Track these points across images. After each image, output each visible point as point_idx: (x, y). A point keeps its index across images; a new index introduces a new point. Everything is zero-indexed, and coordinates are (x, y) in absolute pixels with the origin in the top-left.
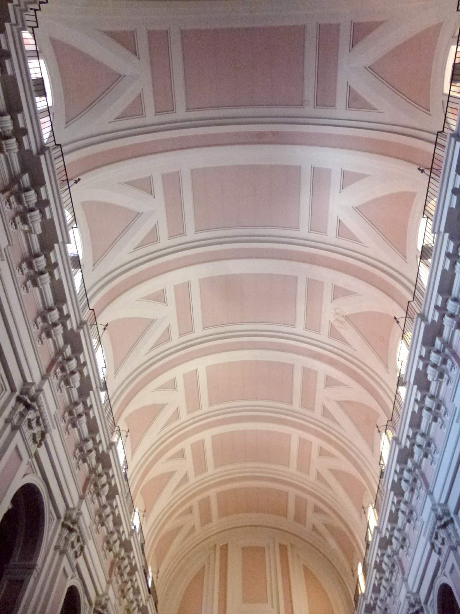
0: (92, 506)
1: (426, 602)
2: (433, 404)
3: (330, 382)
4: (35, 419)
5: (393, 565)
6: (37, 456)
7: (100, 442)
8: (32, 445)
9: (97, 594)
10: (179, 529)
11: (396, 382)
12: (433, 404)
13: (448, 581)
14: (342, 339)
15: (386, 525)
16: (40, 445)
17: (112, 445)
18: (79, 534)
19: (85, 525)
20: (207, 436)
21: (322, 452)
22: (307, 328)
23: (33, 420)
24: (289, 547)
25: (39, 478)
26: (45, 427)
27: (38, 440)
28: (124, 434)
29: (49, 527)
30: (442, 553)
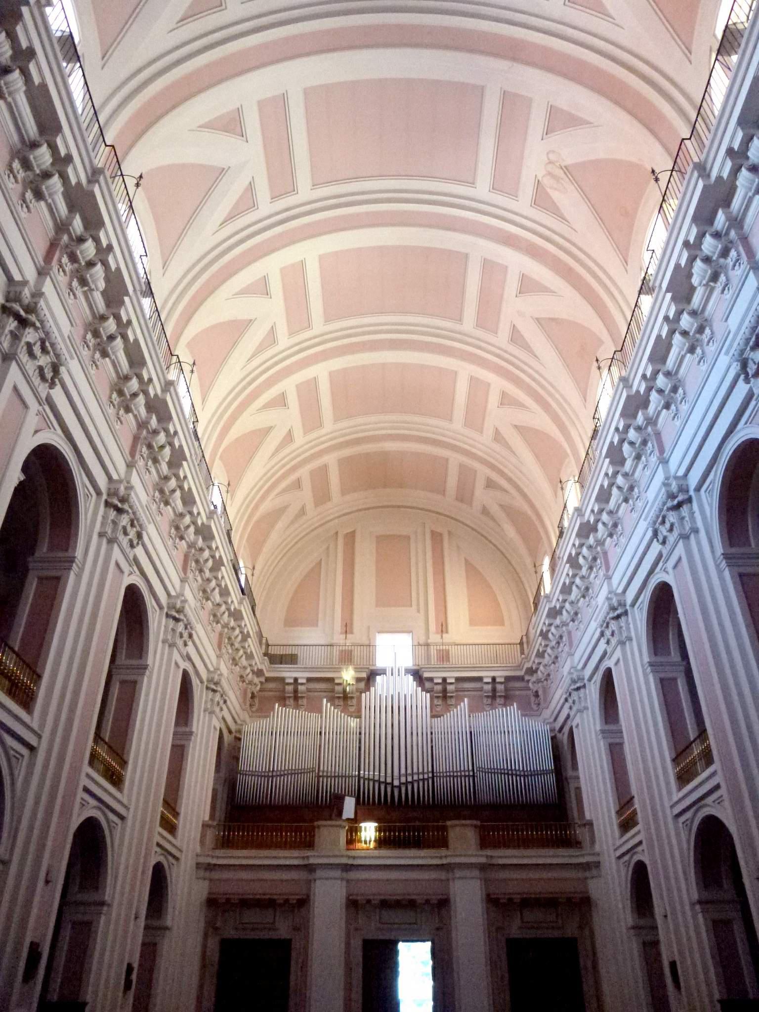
0: (147, 477)
3: (527, 286)
4: (39, 343)
6: (50, 402)
7: (150, 380)
8: (39, 384)
11: (638, 288)
13: (670, 579)
14: (527, 347)
15: (592, 504)
16: (52, 385)
18: (132, 516)
19: (62, 335)
20: (321, 371)
22: (494, 188)
23: (35, 344)
25: (137, 576)
26: (57, 356)
27: (49, 375)
28: (187, 368)
29: (85, 506)
30: (667, 542)
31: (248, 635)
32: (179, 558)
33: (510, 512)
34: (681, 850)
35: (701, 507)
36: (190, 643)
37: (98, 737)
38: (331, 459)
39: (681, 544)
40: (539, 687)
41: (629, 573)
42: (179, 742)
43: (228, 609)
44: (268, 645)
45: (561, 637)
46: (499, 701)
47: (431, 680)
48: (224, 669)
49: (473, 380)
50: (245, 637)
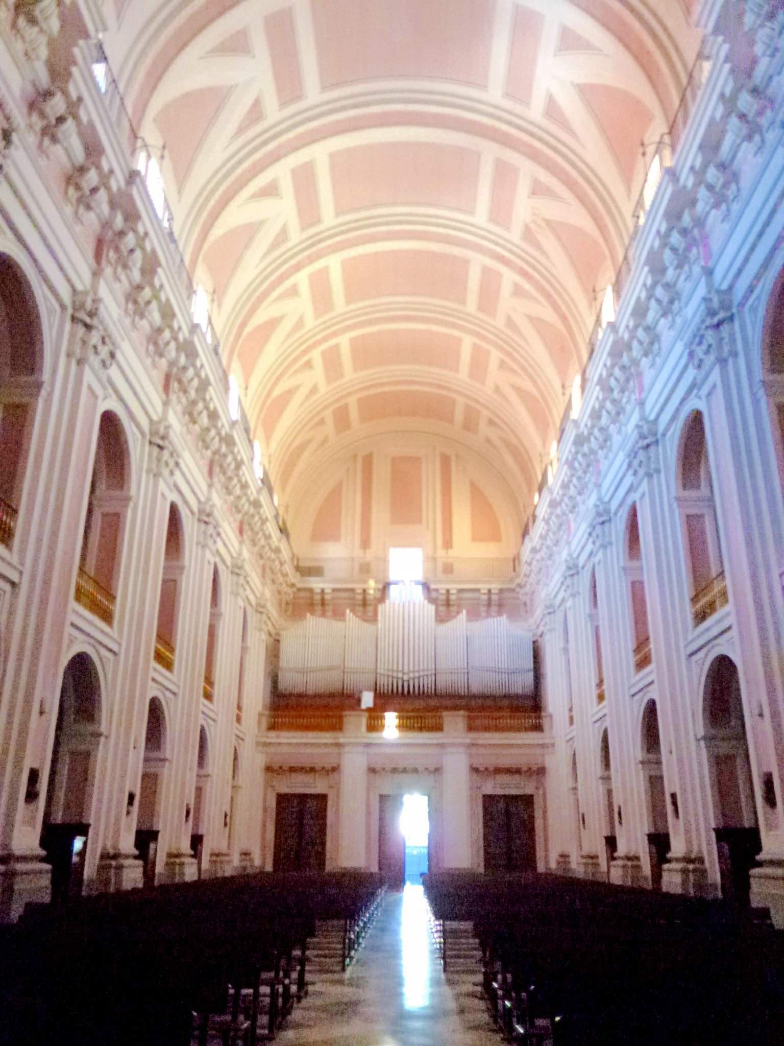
0: (117, 286)
1: (583, 568)
2: (718, 179)
5: (561, 525)
7: (111, 172)
9: (232, 557)
10: (309, 441)
12: (718, 179)
14: (538, 246)
15: (627, 320)
17: (133, 176)
20: (334, 264)
21: (518, 291)
22: (507, 95)
24: (453, 458)
31: (267, 519)
32: (159, 378)
33: (507, 444)
34: (690, 681)
35: (743, 328)
36: (218, 540)
37: (81, 569)
38: (352, 401)
39: (717, 370)
40: (527, 599)
41: (661, 401)
42: (169, 577)
43: (219, 434)
44: (298, 560)
45: (540, 569)
46: (494, 609)
47: (437, 590)
48: (246, 554)
49: (486, 271)
50: (264, 521)
